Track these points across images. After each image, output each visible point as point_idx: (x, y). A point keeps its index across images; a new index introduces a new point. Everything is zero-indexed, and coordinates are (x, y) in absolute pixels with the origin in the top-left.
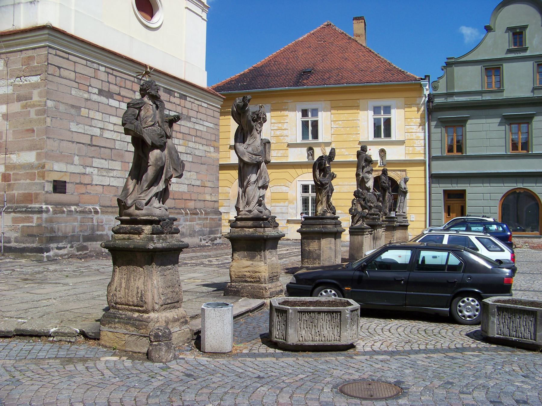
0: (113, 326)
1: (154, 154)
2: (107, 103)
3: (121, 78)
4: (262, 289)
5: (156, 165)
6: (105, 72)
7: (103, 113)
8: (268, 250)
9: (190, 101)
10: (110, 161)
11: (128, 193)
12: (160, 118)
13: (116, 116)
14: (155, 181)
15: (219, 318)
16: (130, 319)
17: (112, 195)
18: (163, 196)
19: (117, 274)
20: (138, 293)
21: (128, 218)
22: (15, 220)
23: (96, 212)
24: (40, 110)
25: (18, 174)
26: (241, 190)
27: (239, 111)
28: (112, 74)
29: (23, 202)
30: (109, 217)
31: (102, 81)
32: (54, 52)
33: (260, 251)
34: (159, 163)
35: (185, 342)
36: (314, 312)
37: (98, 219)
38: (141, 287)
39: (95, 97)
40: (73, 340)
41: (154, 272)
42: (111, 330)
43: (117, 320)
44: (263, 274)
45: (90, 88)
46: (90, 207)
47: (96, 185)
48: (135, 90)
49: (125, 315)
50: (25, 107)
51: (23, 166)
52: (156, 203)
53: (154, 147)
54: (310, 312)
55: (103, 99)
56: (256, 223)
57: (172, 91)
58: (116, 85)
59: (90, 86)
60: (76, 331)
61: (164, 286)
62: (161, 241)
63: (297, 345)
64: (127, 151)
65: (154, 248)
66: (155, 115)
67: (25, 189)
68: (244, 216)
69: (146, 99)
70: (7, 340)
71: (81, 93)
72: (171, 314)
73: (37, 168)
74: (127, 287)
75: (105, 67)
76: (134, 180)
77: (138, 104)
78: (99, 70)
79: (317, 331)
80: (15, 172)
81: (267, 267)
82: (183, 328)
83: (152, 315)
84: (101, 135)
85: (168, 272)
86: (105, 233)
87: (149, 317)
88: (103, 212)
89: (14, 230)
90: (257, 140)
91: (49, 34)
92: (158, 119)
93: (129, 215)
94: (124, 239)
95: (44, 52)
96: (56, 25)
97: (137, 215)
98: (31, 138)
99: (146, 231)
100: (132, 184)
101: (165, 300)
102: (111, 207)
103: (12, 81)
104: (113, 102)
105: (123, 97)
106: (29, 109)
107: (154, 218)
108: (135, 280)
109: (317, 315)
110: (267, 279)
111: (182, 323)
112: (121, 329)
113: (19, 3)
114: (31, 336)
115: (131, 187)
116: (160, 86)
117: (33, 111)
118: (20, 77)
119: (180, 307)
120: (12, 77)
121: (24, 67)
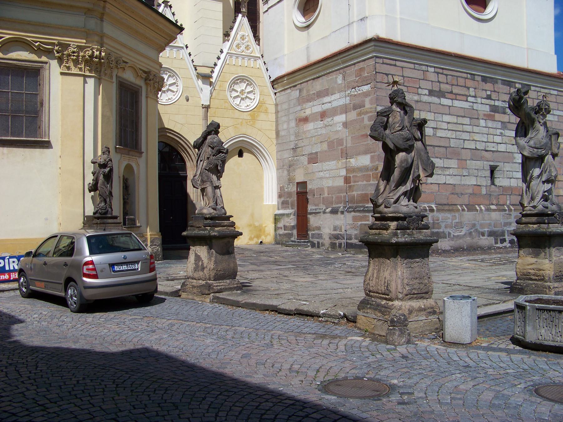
0: (366, 311)
1: (400, 157)
2: (439, 102)
3: (452, 76)
4: (546, 288)
5: (400, 166)
6: (435, 72)
7: (435, 113)
8: (554, 247)
9: (535, 91)
10: (445, 160)
11: (379, 193)
12: (409, 122)
13: (449, 114)
14: (402, 181)
15: (457, 310)
16: (379, 305)
17: (449, 193)
18: (414, 194)
19: (372, 265)
20: (385, 282)
21: (379, 215)
22: (355, 219)
23: (432, 210)
24: (371, 116)
25: (356, 176)
26: (524, 185)
27: (517, 105)
28: (442, 74)
29: (360, 202)
30: (445, 215)
31: (432, 81)
32: (381, 61)
33: (545, 248)
34: (403, 165)
35: (433, 332)
36: (554, 311)
37: (433, 217)
38: (388, 277)
39: (426, 99)
40: (336, 322)
41: (399, 264)
42: (365, 314)
43: (368, 306)
44: (547, 272)
45: (420, 90)
46: (426, 205)
47: (431, 184)
48: (469, 86)
49: (376, 302)
50: (359, 114)
51: (360, 169)
52: (404, 201)
53: (399, 150)
54: (549, 310)
55: (435, 100)
56: (540, 219)
57: (512, 82)
58: (447, 83)
59: (420, 87)
60: (340, 314)
61: (410, 277)
62: (406, 236)
63: (535, 344)
64: (463, 148)
65: (396, 242)
66: (402, 121)
67: (363, 190)
68: (529, 212)
69: (394, 107)
70: (290, 317)
71: (411, 96)
72: (416, 304)
73: (371, 170)
74: (378, 278)
75: (434, 67)
76: (385, 181)
77: (386, 112)
78: (428, 71)
79: (558, 331)
80: (354, 174)
81: (552, 266)
82: (430, 317)
83: (396, 303)
84: (435, 135)
85: (416, 265)
86: (441, 230)
87: (393, 305)
88: (438, 210)
89: (354, 228)
90: (540, 132)
91: (375, 46)
92: (407, 123)
93: (380, 212)
94: (376, 234)
95: (372, 62)
96: (383, 35)
97: (386, 213)
98: (365, 143)
99: (392, 227)
100: (382, 184)
101: (411, 290)
102: (448, 205)
103: (349, 92)
104: (444, 101)
105: (456, 94)
106: (363, 116)
107: (399, 215)
108: (384, 271)
109: (557, 315)
110: (551, 278)
111: (430, 313)
112: (372, 314)
113: (352, 23)
114: (307, 315)
115: (382, 188)
116: (497, 79)
117: (366, 117)
118: (355, 88)
119: (430, 298)
120: (348, 89)
121: (357, 79)
